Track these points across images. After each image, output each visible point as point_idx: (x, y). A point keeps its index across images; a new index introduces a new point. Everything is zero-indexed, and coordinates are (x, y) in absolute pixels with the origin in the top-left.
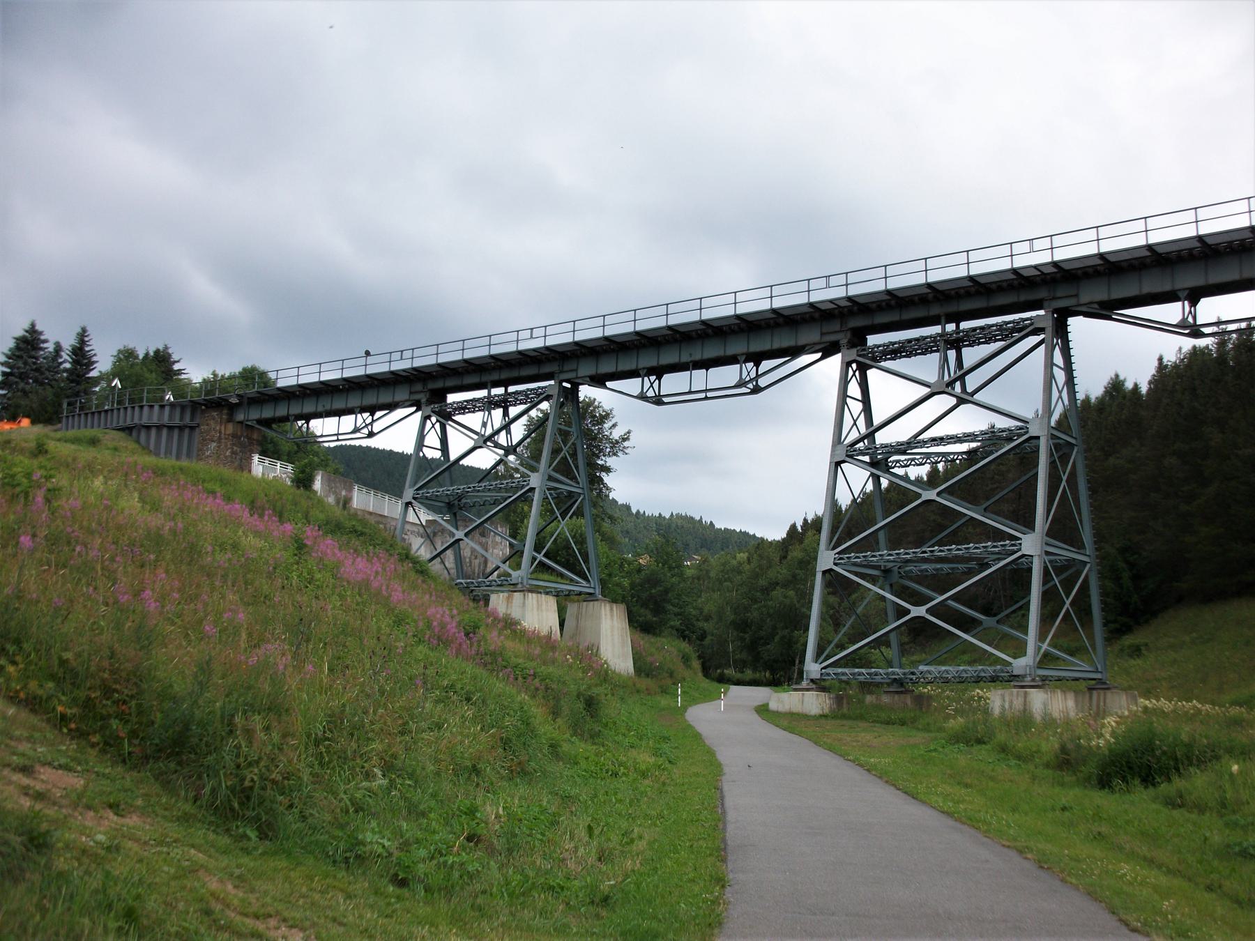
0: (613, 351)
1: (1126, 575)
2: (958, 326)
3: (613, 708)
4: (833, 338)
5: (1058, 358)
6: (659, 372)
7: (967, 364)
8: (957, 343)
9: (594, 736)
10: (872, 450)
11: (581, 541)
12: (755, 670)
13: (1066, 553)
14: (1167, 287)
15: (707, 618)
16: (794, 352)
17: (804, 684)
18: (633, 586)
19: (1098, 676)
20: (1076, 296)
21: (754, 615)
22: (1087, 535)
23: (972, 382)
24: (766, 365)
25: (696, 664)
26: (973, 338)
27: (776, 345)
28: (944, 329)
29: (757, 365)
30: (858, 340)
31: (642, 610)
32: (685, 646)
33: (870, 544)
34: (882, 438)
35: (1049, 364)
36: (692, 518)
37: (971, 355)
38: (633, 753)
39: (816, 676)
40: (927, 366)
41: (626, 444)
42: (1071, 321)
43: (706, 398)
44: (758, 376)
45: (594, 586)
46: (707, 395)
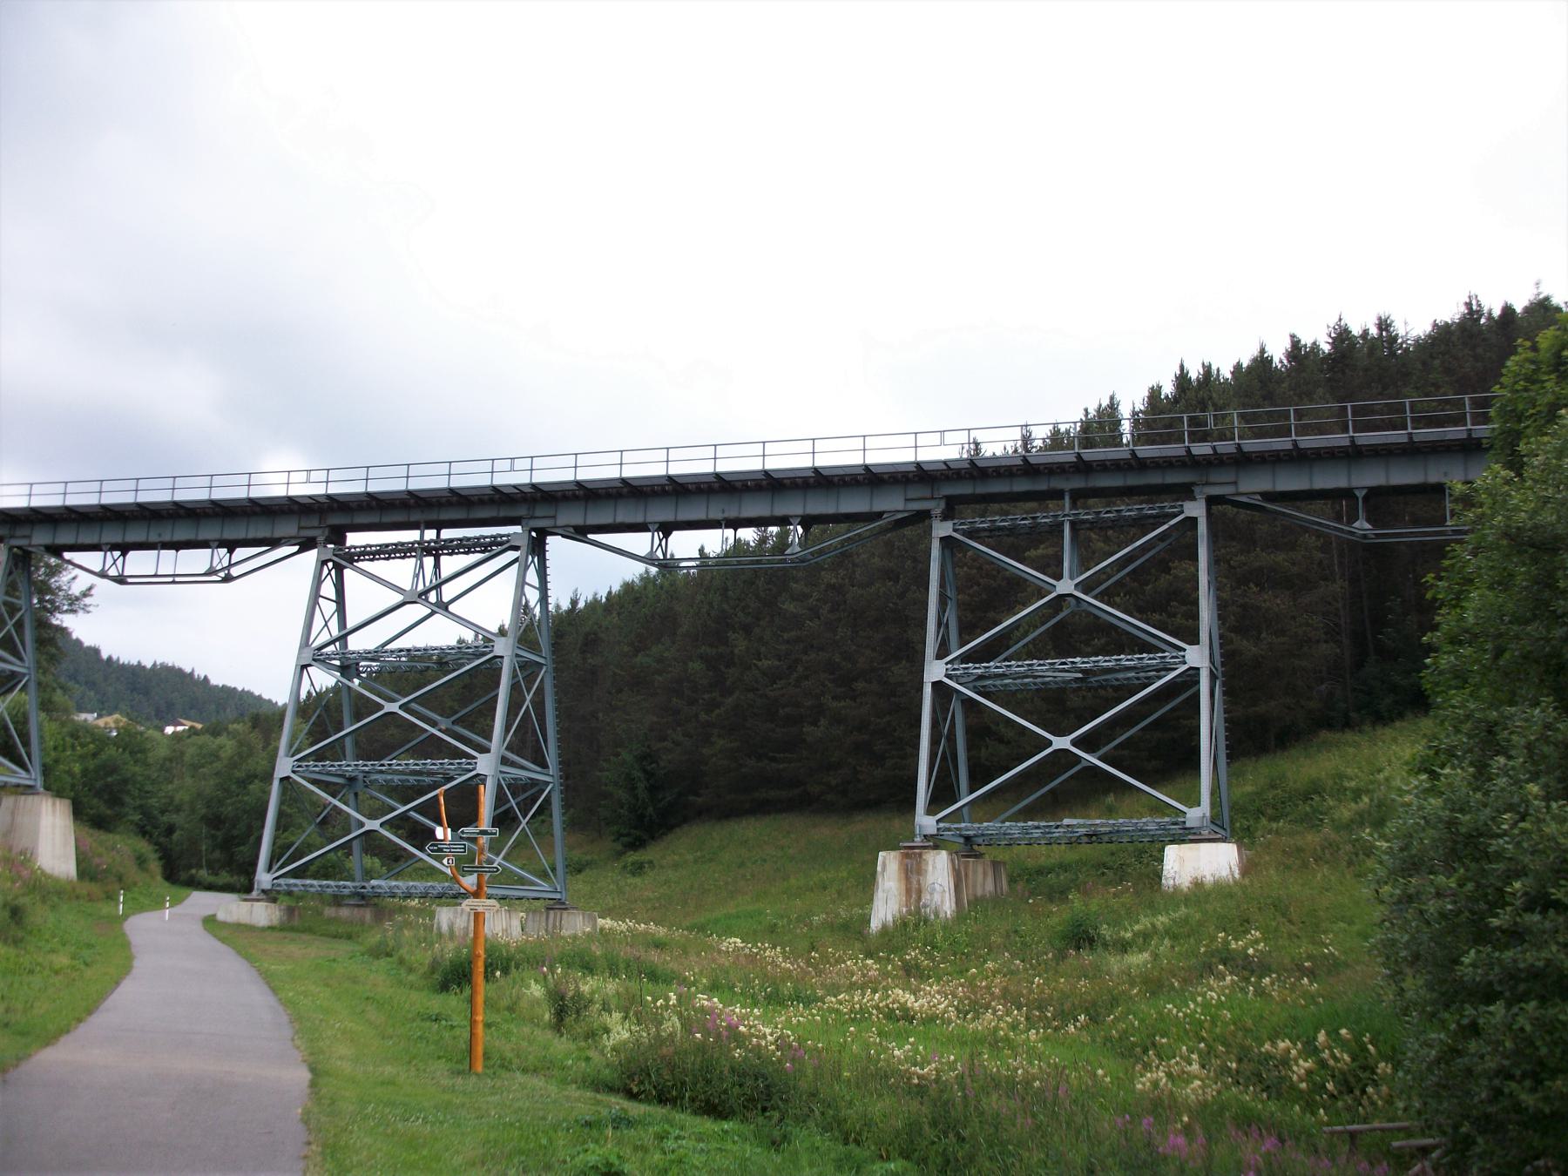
0: (74, 520)
1: (641, 786)
2: (438, 534)
3: (39, 915)
4: (310, 533)
5: (532, 576)
6: (125, 549)
7: (445, 573)
8: (436, 550)
9: (16, 942)
10: (344, 655)
11: (22, 722)
12: (231, 872)
13: (528, 772)
14: (639, 519)
15: (178, 810)
16: (274, 543)
17: (254, 894)
18: (85, 772)
19: (558, 896)
20: (554, 517)
21: (228, 810)
22: (552, 757)
23: (449, 592)
24: (240, 553)
25: (155, 866)
26: (454, 547)
27: (251, 535)
28: (422, 535)
29: (231, 552)
30: (338, 536)
31: (95, 801)
32: (144, 846)
33: (334, 752)
34: (357, 643)
35: (521, 583)
36: (180, 670)
37: (450, 564)
38: (53, 957)
39: (267, 886)
40: (401, 571)
41: (87, 601)
42: (549, 539)
43: (174, 582)
44: (231, 565)
45: (34, 777)
46: (174, 579)
